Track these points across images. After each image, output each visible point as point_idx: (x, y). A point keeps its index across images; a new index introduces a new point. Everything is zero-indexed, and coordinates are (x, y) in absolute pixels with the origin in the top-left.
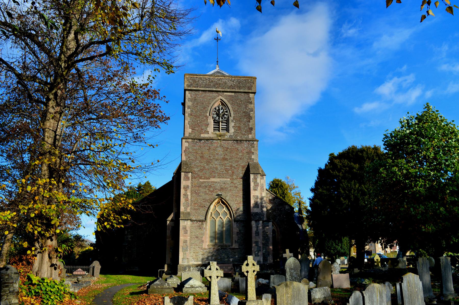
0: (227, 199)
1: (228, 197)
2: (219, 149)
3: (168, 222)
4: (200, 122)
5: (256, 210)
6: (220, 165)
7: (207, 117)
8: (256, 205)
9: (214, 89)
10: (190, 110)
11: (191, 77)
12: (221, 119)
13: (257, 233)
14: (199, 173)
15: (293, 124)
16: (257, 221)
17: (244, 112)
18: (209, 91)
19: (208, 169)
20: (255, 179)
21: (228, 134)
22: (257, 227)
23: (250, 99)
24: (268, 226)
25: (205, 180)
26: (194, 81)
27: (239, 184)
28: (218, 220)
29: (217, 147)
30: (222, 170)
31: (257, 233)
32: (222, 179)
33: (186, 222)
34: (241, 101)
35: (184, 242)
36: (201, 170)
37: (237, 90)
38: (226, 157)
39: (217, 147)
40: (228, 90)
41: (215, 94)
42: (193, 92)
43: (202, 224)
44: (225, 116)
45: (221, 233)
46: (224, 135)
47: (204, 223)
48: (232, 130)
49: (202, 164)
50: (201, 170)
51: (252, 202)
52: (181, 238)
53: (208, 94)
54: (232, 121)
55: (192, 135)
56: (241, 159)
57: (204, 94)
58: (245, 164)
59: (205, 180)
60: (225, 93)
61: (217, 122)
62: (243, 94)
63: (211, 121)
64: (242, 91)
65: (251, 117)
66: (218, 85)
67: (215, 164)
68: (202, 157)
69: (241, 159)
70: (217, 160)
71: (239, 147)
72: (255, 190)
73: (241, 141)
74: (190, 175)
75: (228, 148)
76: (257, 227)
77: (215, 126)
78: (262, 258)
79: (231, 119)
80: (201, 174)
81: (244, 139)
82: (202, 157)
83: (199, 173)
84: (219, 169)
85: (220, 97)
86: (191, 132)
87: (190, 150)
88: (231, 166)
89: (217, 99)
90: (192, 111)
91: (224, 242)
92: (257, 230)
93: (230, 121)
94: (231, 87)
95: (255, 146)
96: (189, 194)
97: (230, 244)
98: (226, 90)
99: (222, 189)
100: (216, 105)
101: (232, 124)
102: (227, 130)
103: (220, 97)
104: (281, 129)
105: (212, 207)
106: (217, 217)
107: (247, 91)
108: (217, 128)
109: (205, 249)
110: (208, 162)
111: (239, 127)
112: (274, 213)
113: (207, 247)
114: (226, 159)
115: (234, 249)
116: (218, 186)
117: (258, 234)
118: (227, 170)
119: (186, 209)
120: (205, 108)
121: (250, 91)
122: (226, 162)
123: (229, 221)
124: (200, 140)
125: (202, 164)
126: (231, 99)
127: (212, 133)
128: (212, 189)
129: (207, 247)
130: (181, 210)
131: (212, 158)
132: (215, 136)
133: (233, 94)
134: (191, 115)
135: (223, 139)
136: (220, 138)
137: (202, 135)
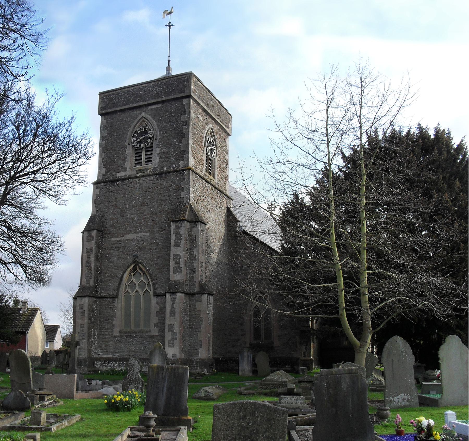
4: (116, 157)
6: (137, 214)
7: (125, 147)
10: (104, 142)
11: (107, 96)
13: (173, 313)
17: (174, 129)
18: (121, 111)
20: (178, 228)
25: (118, 239)
30: (140, 221)
32: (138, 235)
33: (83, 299)
35: (81, 328)
37: (164, 99)
40: (153, 101)
41: (136, 112)
43: (113, 302)
44: (149, 140)
48: (156, 160)
54: (158, 146)
58: (234, 199)
59: (118, 239)
60: (150, 107)
61: (138, 153)
63: (130, 151)
64: (171, 97)
69: (165, 200)
72: (177, 245)
77: (150, 156)
78: (178, 350)
81: (172, 169)
84: (136, 219)
86: (104, 173)
94: (157, 95)
95: (186, 177)
96: (92, 259)
97: (148, 329)
98: (149, 102)
102: (149, 160)
105: (126, 275)
107: (177, 96)
108: (138, 162)
111: (167, 153)
115: (153, 336)
117: (174, 314)
121: (182, 95)
122: (145, 208)
131: (127, 206)
133: (160, 105)
137: (118, 175)
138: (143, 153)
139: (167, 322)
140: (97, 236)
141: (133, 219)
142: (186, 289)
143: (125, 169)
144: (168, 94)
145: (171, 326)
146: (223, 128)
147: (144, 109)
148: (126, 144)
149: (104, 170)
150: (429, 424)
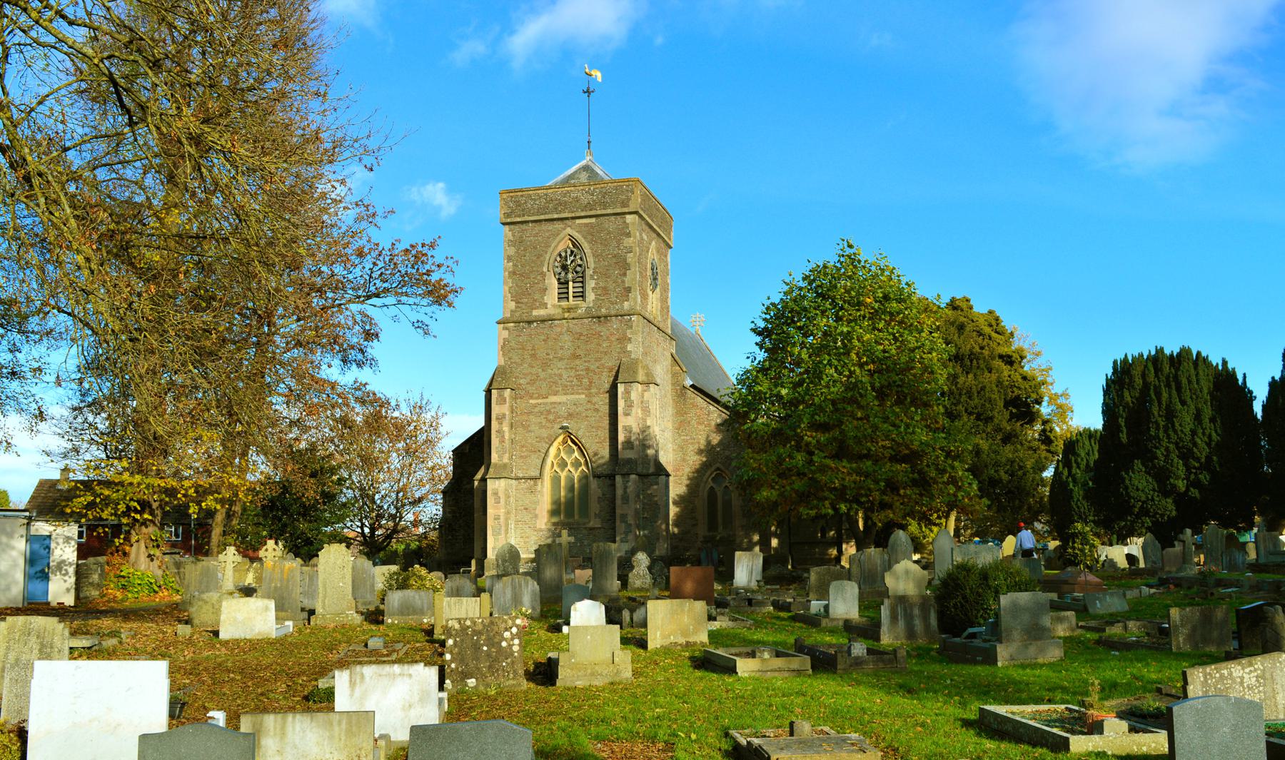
0: (580, 434)
1: (580, 430)
2: (566, 337)
3: (476, 483)
5: (629, 455)
7: (543, 275)
8: (629, 444)
9: (556, 216)
12: (571, 272)
13: (626, 499)
14: (529, 388)
15: (1214, 85)
16: (625, 475)
19: (545, 379)
20: (627, 392)
21: (584, 305)
22: (626, 488)
23: (627, 226)
24: (657, 484)
26: (518, 204)
27: (603, 402)
28: (563, 475)
29: (561, 334)
31: (626, 499)
32: (570, 397)
33: (497, 482)
34: (609, 233)
36: (532, 382)
37: (599, 212)
38: (579, 352)
39: (561, 334)
40: (583, 214)
41: (558, 225)
42: (516, 227)
44: (578, 269)
45: (570, 503)
46: (577, 307)
47: (539, 482)
48: (591, 296)
49: (534, 371)
50: (532, 382)
51: (621, 437)
52: (490, 511)
53: (545, 226)
55: (517, 314)
56: (606, 353)
57: (537, 227)
58: (611, 363)
60: (578, 221)
61: (563, 283)
62: (613, 218)
64: (609, 211)
65: (629, 265)
66: (561, 205)
67: (558, 368)
68: (533, 356)
69: (606, 353)
70: (561, 359)
71: (603, 330)
72: (627, 415)
73: (606, 317)
74: (507, 393)
75: (581, 334)
76: (626, 488)
79: (589, 272)
80: (531, 389)
81: (613, 312)
82: (533, 356)
83: (529, 388)
84: (565, 376)
85: (569, 230)
87: (513, 344)
88: (587, 369)
89: (562, 235)
90: (515, 265)
91: (576, 517)
92: (625, 492)
93: (587, 278)
94: (589, 206)
96: (506, 429)
99: (570, 416)
100: (561, 247)
101: (590, 284)
102: (582, 296)
103: (569, 230)
104: (1174, 110)
105: (553, 451)
106: (562, 470)
107: (619, 211)
108: (563, 295)
109: (541, 530)
110: (545, 365)
111: (605, 289)
112: (727, 453)
113: (543, 527)
114: (578, 357)
115: (591, 529)
116: (563, 411)
118: (579, 378)
119: (500, 457)
120: (539, 256)
121: (626, 210)
122: (578, 362)
123: (584, 477)
124: (530, 322)
125: (534, 371)
126: (590, 233)
127: (554, 306)
128: (551, 417)
129: (543, 527)
130: (493, 461)
132: (560, 311)
133: (593, 220)
134: (514, 273)
135: (573, 315)
136: (566, 315)
137: (535, 313)
138: (571, 284)
139: (618, 512)
140: (511, 397)
141: (560, 376)
142: (639, 470)
143: (545, 306)
144: (605, 206)
145: (624, 516)
146: (664, 241)
147: (569, 222)
148: (545, 269)
149: (512, 305)
150: (13, 548)
